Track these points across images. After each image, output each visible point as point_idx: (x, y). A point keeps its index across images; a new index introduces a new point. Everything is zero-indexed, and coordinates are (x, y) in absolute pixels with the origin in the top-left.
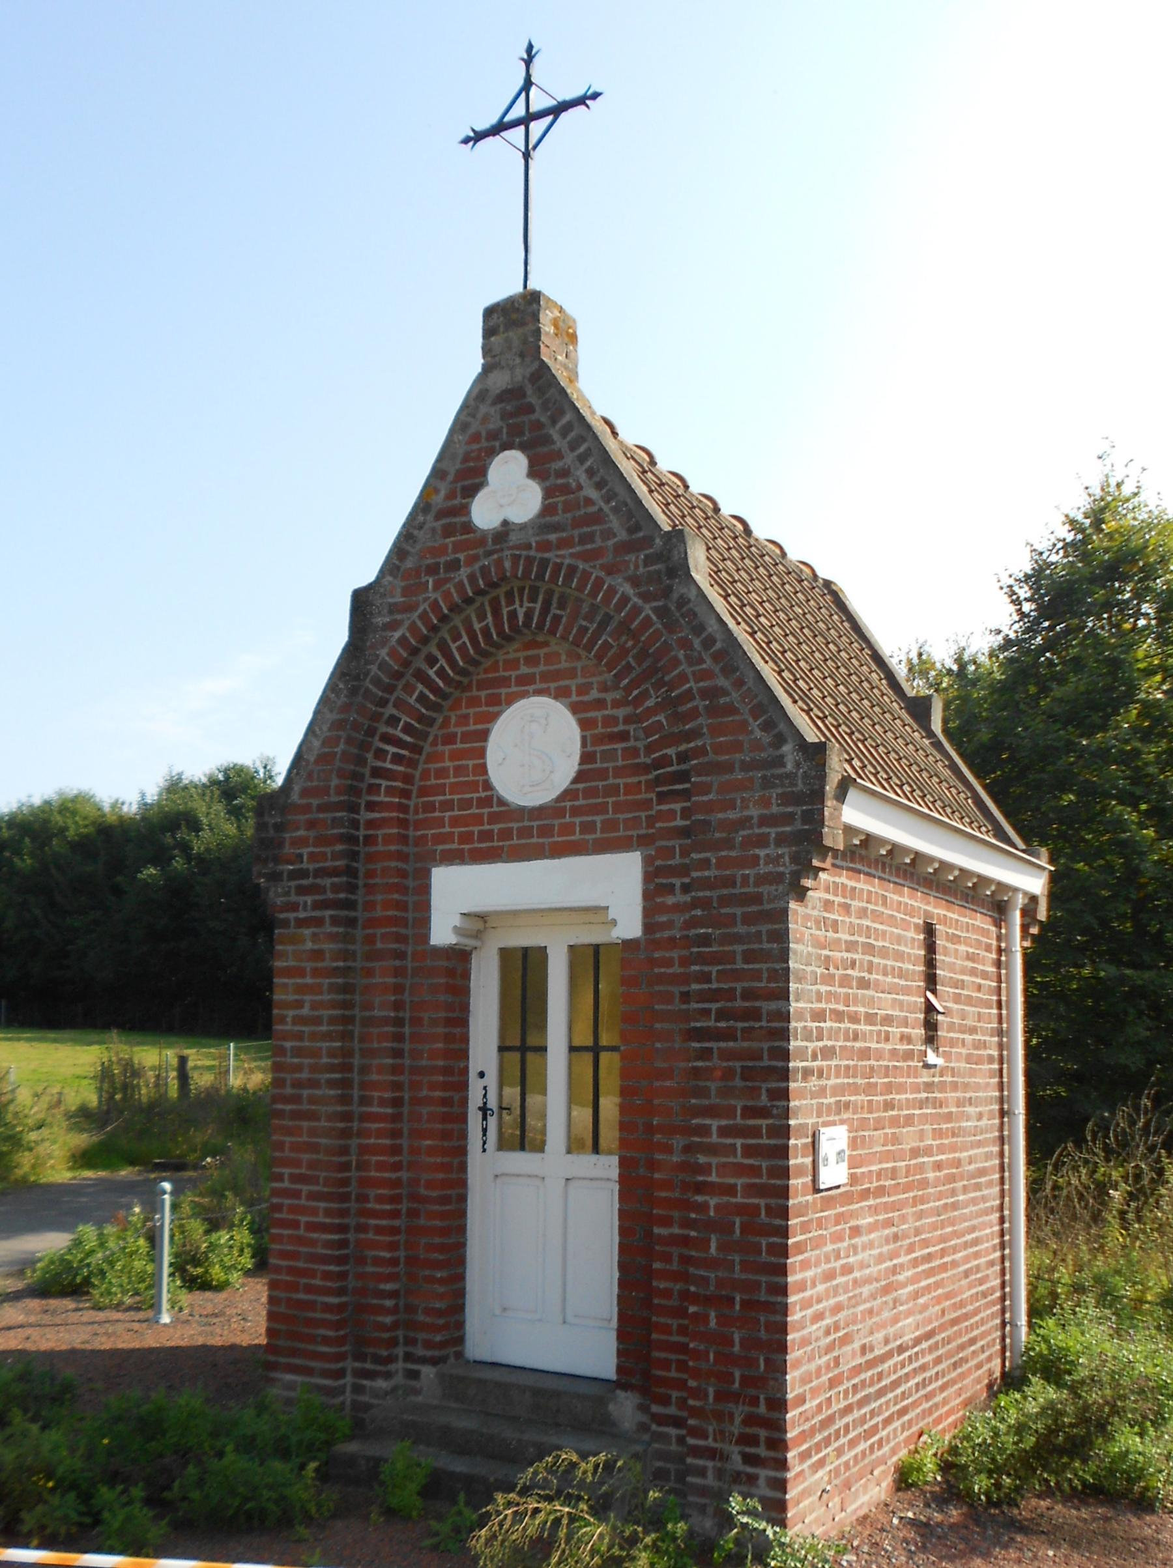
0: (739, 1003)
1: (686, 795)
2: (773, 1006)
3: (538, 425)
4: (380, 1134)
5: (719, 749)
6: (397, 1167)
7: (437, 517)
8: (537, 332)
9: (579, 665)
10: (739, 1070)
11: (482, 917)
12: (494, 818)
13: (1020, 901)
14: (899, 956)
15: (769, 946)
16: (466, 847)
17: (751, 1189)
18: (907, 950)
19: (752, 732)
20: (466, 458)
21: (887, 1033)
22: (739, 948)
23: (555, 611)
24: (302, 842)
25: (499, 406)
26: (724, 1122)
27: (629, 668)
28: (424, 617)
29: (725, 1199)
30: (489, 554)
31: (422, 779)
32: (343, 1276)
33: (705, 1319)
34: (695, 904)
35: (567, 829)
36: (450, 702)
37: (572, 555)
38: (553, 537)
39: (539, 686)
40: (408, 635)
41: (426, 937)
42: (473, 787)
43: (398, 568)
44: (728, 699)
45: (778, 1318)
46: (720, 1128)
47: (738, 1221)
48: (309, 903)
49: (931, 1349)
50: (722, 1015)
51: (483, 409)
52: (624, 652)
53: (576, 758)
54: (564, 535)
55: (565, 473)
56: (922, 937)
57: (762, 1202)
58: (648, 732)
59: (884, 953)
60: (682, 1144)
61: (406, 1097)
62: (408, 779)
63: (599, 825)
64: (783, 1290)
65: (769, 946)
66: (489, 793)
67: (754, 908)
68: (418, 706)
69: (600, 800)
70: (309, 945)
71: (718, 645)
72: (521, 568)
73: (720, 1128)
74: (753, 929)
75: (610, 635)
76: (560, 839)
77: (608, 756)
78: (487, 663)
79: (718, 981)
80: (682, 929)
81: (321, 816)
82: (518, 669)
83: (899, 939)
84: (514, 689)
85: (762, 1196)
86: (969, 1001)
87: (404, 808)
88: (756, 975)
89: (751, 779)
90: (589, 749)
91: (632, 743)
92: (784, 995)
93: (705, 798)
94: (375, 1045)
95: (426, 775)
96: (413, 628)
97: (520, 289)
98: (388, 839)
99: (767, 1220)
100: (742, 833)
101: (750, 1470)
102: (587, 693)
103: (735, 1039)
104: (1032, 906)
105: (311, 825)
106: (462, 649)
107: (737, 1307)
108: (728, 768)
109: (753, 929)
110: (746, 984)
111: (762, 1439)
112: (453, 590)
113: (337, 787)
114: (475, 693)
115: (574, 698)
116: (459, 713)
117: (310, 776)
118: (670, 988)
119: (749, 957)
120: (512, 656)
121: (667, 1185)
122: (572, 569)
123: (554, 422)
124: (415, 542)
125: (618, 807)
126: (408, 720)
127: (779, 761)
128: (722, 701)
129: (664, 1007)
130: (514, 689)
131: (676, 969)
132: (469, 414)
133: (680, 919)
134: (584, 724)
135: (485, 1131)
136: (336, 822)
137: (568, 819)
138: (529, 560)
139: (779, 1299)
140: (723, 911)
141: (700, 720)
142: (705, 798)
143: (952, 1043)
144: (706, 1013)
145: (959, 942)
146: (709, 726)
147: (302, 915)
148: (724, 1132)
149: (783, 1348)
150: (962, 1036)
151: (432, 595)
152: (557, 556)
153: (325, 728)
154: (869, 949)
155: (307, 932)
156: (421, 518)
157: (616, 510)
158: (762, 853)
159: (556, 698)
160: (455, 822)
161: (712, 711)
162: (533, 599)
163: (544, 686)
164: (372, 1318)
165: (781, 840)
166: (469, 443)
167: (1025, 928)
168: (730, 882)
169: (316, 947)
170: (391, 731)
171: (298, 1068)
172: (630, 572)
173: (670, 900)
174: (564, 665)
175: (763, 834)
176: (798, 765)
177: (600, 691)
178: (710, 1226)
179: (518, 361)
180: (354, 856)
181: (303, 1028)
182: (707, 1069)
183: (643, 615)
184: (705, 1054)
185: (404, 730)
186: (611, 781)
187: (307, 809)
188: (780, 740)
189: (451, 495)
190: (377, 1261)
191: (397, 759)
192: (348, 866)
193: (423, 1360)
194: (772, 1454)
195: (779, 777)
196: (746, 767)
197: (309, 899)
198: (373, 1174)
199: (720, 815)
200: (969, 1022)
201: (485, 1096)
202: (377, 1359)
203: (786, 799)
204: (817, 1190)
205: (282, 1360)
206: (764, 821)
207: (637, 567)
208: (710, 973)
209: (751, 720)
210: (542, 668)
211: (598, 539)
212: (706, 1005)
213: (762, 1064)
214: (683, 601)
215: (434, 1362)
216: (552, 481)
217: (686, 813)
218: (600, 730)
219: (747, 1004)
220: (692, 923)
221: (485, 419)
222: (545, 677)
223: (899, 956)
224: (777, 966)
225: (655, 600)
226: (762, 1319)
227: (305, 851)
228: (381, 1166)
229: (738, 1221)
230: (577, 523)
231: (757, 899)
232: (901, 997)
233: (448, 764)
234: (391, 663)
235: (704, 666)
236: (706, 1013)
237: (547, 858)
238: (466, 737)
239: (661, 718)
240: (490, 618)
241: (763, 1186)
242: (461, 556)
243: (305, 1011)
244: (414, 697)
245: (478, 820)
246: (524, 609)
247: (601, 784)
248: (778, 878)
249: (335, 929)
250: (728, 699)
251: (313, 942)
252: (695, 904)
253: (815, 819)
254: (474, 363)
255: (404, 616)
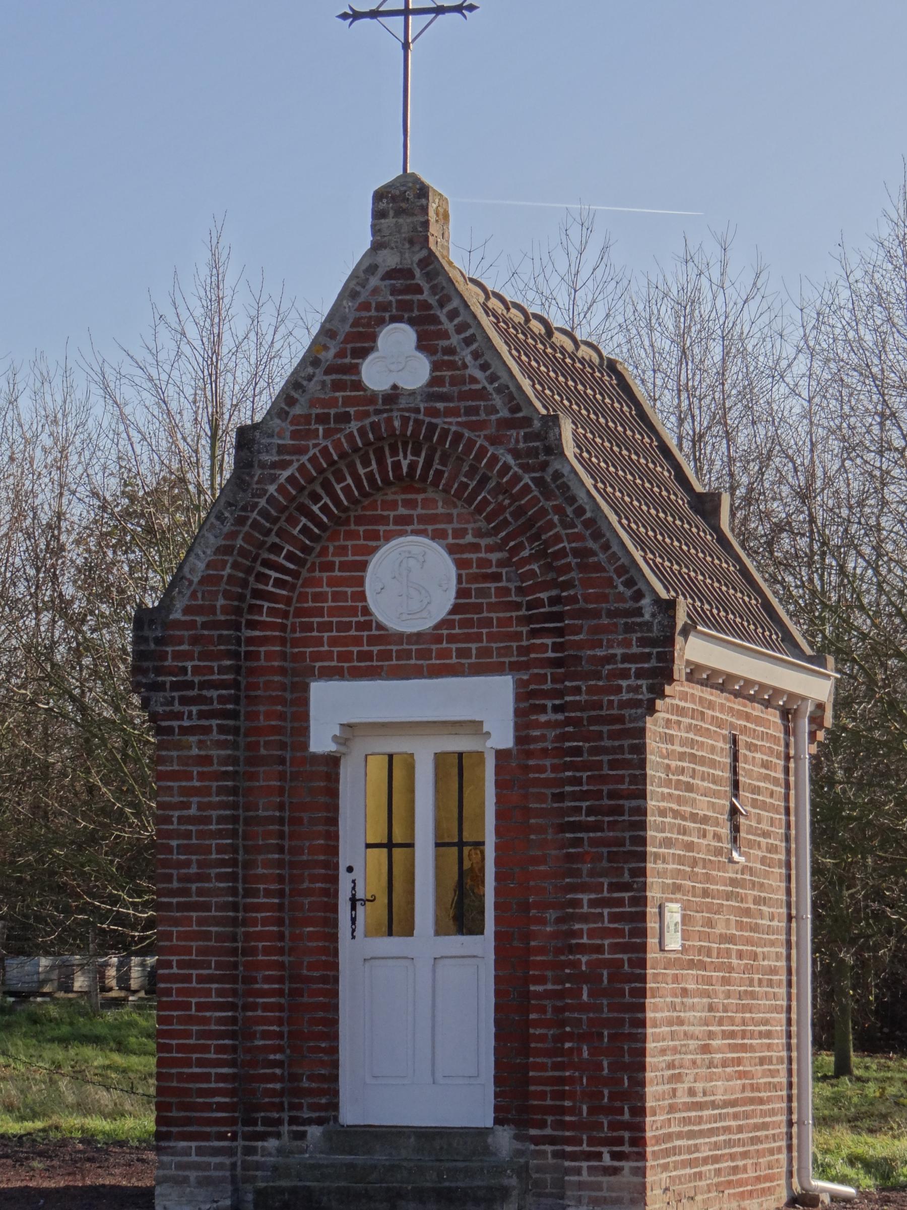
0: (606, 802)
1: (560, 632)
2: (634, 803)
3: (425, 306)
4: (265, 922)
5: (587, 598)
6: (281, 951)
7: (327, 372)
8: (426, 224)
9: (455, 512)
10: (605, 855)
11: (350, 726)
12: (372, 640)
13: (810, 708)
14: (713, 764)
15: (630, 756)
16: (346, 665)
17: (615, 948)
18: (718, 759)
19: (616, 587)
20: (356, 323)
21: (705, 830)
22: (605, 758)
23: (436, 466)
24: (187, 656)
25: (388, 282)
26: (593, 896)
27: (506, 523)
28: (313, 460)
29: (595, 956)
30: (378, 412)
31: (298, 601)
32: (234, 1049)
33: (580, 1050)
34: (568, 722)
35: (444, 654)
36: (328, 534)
37: (458, 424)
38: (440, 405)
39: (416, 526)
40: (297, 475)
41: (305, 745)
42: (353, 611)
43: (287, 413)
44: (596, 559)
45: (639, 1045)
46: (590, 900)
47: (605, 973)
48: (194, 712)
49: (736, 1116)
50: (590, 811)
51: (374, 281)
52: (501, 509)
53: (453, 593)
54: (451, 405)
55: (450, 351)
56: (728, 746)
57: (625, 957)
58: (523, 577)
59: (702, 761)
60: (553, 917)
61: (287, 890)
62: (288, 601)
63: (474, 652)
64: (642, 1023)
65: (630, 756)
66: (367, 618)
67: (618, 727)
68: (301, 537)
69: (475, 630)
70: (195, 751)
71: (588, 515)
72: (410, 429)
73: (590, 900)
74: (617, 743)
75: (489, 493)
76: (438, 662)
77: (482, 593)
78: (366, 502)
79: (588, 784)
80: (553, 742)
81: (206, 632)
82: (396, 509)
83: (713, 749)
84: (391, 527)
85: (624, 952)
86: (764, 806)
87: (283, 628)
88: (620, 779)
89: (615, 625)
90: (464, 585)
91: (503, 584)
92: (643, 795)
93: (576, 638)
94: (261, 843)
95: (303, 597)
96: (302, 469)
97: (401, 173)
98: (269, 656)
99: (629, 970)
100: (607, 667)
101: (616, 1164)
102: (463, 537)
103: (602, 830)
104: (819, 713)
105: (195, 640)
106: (347, 490)
107: (606, 1040)
108: (596, 614)
109: (617, 743)
110: (611, 787)
111: (627, 1139)
112: (343, 440)
113: (222, 606)
114: (353, 527)
115: (450, 540)
116: (337, 544)
117: (194, 595)
118: (543, 790)
119: (613, 765)
120: (390, 497)
121: (542, 950)
122: (458, 437)
123: (442, 305)
124: (304, 391)
125: (491, 637)
126: (291, 549)
127: (639, 612)
128: (591, 560)
129: (538, 806)
130: (391, 527)
131: (549, 775)
132: (358, 284)
133: (552, 734)
134: (460, 564)
135: (353, 920)
136: (221, 639)
137: (445, 645)
138: (418, 423)
139: (640, 1031)
140: (592, 728)
141: (573, 574)
142: (576, 638)
143: (751, 844)
144: (578, 810)
145: (756, 751)
146: (580, 579)
147: (186, 723)
148: (593, 904)
149: (642, 1068)
150: (758, 839)
151: (324, 443)
152: (445, 423)
153: (209, 552)
154: (693, 758)
155: (193, 739)
156: (310, 370)
157: (499, 390)
158: (624, 683)
159: (433, 539)
160: (333, 642)
161: (582, 567)
162: (416, 453)
163: (422, 527)
164: (263, 1086)
165: (639, 674)
166: (358, 310)
167: (812, 736)
168: (598, 705)
169: (203, 753)
170: (273, 557)
171: (187, 864)
172: (511, 446)
173: (543, 718)
174: (440, 510)
175: (625, 669)
176: (653, 615)
177: (474, 536)
178: (581, 978)
179: (407, 246)
180: (237, 670)
181: (190, 827)
182: (578, 854)
183: (522, 484)
184: (578, 842)
185: (287, 558)
186: (485, 614)
187: (192, 625)
188: (639, 595)
189: (341, 354)
190: (265, 1035)
191: (279, 583)
192: (235, 679)
193: (309, 1122)
194: (635, 1149)
195: (640, 625)
196: (611, 614)
197: (194, 709)
198: (260, 958)
199: (589, 652)
200: (765, 826)
201: (354, 888)
202: (267, 1122)
203: (643, 642)
204: (662, 950)
205: (174, 1129)
206: (626, 658)
207: (517, 441)
208: (581, 777)
209: (615, 577)
210: (419, 511)
211: (482, 412)
212: (577, 804)
213: (625, 849)
214: (557, 475)
215: (320, 1122)
216: (439, 356)
217: (557, 647)
218: (474, 570)
219: (612, 802)
220: (564, 737)
221: (375, 291)
222: (423, 519)
223: (713, 764)
224: (637, 772)
225: (534, 471)
226: (626, 1047)
227: (189, 665)
228: (267, 951)
229: (605, 973)
230: (463, 396)
231: (620, 719)
232: (713, 800)
233: (325, 589)
234: (281, 499)
235: (576, 530)
236: (578, 810)
237: (425, 677)
238: (344, 566)
239: (535, 567)
240: (374, 466)
241: (625, 944)
242: (352, 410)
243: (193, 811)
244: (298, 528)
245: (357, 641)
246: (407, 461)
247: (475, 616)
248: (637, 704)
249: (223, 737)
250: (596, 559)
251: (200, 749)
252: (568, 722)
253: (667, 659)
254: (365, 241)
255: (294, 458)
